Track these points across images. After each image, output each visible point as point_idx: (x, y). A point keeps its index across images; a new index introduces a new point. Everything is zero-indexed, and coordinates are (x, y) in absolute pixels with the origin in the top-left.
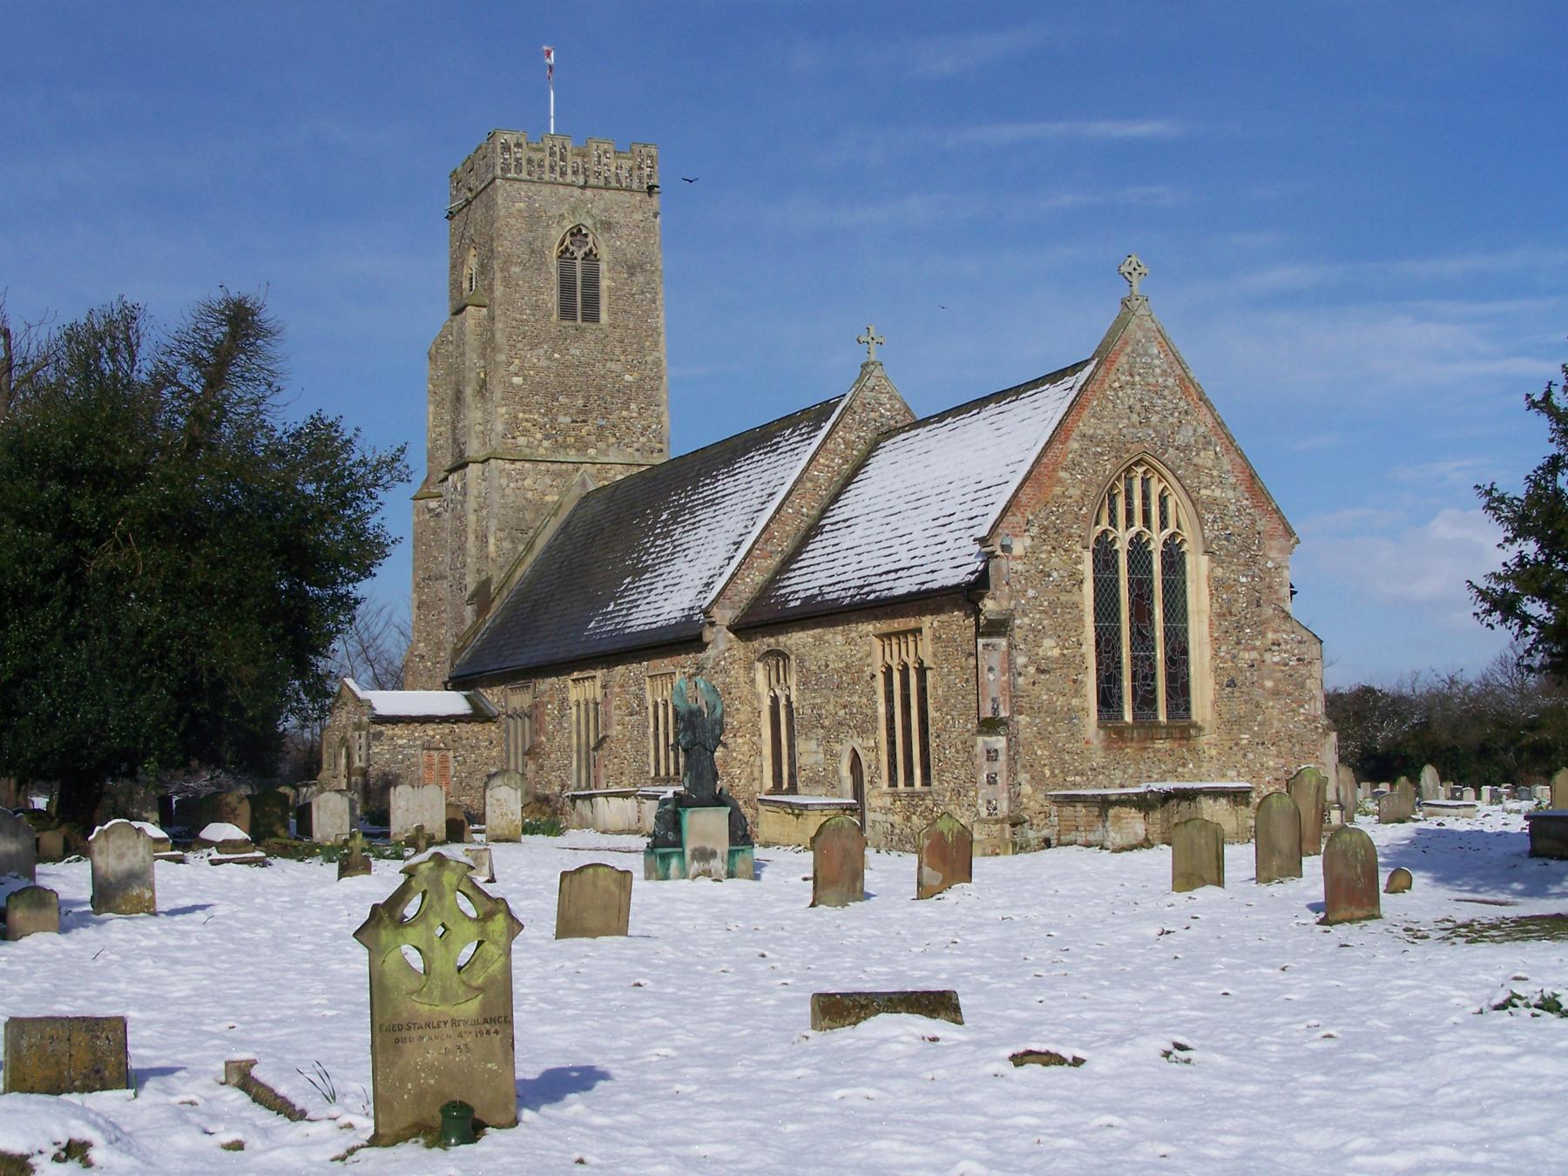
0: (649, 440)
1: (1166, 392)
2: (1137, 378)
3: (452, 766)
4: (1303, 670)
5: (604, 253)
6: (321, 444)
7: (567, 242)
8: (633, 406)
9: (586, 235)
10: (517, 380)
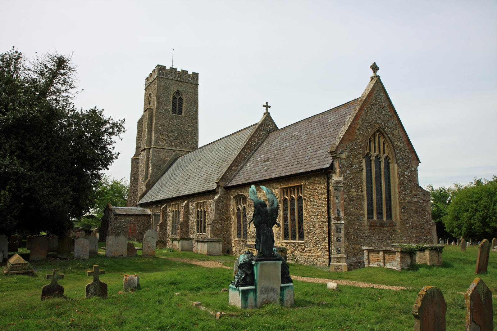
0: (193, 146)
1: (385, 109)
2: (377, 102)
3: (137, 228)
4: (425, 204)
5: (184, 98)
6: (94, 120)
7: (175, 94)
8: (190, 137)
9: (180, 93)
10: (160, 128)
